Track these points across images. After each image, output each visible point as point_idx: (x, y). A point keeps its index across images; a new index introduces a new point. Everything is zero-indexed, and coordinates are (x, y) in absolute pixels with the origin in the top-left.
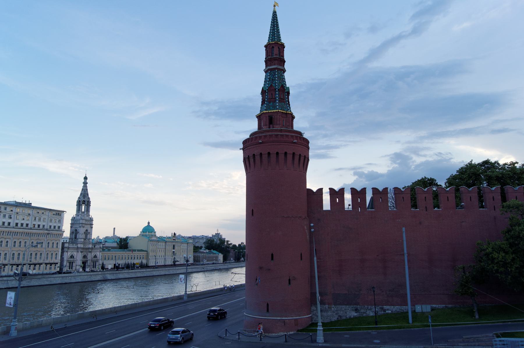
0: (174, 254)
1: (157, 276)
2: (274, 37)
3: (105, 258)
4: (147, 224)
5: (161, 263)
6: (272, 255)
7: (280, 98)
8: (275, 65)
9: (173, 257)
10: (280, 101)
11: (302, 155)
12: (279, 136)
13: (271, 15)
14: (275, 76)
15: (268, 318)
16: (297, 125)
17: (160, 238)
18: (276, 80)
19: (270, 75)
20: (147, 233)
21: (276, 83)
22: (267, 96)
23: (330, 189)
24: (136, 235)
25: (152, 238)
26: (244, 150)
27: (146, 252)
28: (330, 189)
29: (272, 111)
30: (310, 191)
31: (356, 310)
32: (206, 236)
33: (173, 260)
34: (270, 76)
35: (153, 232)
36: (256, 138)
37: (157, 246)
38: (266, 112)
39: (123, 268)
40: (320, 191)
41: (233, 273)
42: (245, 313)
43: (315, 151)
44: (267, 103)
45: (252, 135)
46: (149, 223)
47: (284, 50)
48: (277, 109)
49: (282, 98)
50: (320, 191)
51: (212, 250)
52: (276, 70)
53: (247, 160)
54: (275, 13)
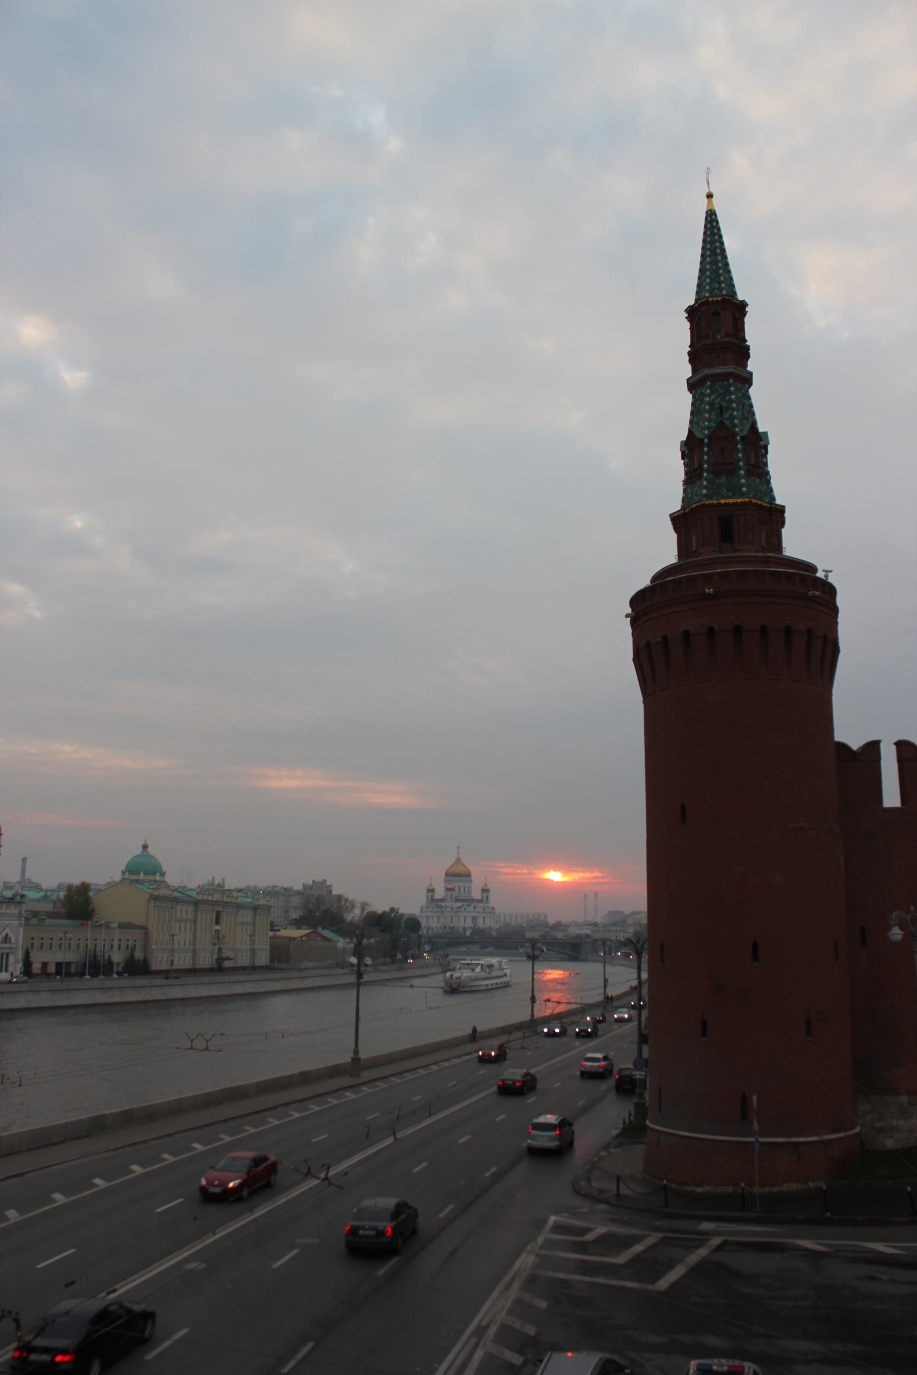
0: (218, 938)
1: (182, 999)
2: (716, 285)
3: (42, 943)
4: (139, 850)
5: (183, 961)
6: (755, 946)
7: (748, 464)
8: (725, 363)
9: (217, 947)
10: (749, 474)
14: (727, 398)
17: (180, 890)
18: (733, 409)
19: (712, 393)
20: (142, 876)
21: (732, 418)
22: (707, 454)
25: (159, 889)
27: (143, 931)
29: (731, 501)
30: (843, 748)
32: (285, 889)
33: (215, 956)
34: (713, 397)
35: (158, 874)
37: (174, 914)
38: (743, 500)
39: (81, 974)
40: (873, 748)
41: (549, 1000)
42: (651, 1122)
44: (711, 476)
45: (659, 577)
46: (145, 847)
48: (742, 495)
50: (873, 748)
52: (731, 380)
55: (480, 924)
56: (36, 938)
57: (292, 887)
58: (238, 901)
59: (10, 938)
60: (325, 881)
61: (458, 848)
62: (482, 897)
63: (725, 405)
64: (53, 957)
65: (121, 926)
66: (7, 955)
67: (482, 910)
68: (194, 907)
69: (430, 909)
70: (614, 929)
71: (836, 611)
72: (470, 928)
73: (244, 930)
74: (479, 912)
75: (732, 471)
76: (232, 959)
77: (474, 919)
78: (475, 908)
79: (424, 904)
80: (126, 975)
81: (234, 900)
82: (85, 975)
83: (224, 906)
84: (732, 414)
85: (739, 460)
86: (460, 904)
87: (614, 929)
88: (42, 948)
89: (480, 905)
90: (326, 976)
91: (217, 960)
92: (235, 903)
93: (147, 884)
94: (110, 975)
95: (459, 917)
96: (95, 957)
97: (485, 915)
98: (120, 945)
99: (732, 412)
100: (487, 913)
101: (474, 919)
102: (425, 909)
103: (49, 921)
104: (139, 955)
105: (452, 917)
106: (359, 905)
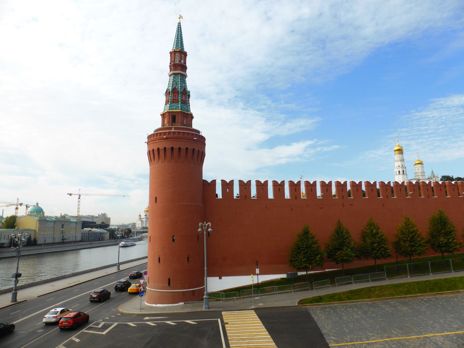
0: (63, 232)
8: (178, 70)
9: (62, 235)
10: (182, 103)
11: (200, 151)
12: (177, 133)
13: (176, 27)
16: (195, 125)
23: (222, 180)
24: (159, 126)
26: (149, 144)
28: (222, 180)
30: (205, 182)
32: (92, 216)
33: (61, 238)
36: (161, 134)
39: (10, 247)
40: (214, 182)
42: (149, 288)
43: (391, 136)
46: (37, 204)
47: (186, 58)
49: (184, 100)
50: (214, 182)
53: (151, 153)
54: (180, 24)
60: (105, 213)
68: (54, 223)
71: (205, 144)
83: (69, 222)
90: (99, 243)
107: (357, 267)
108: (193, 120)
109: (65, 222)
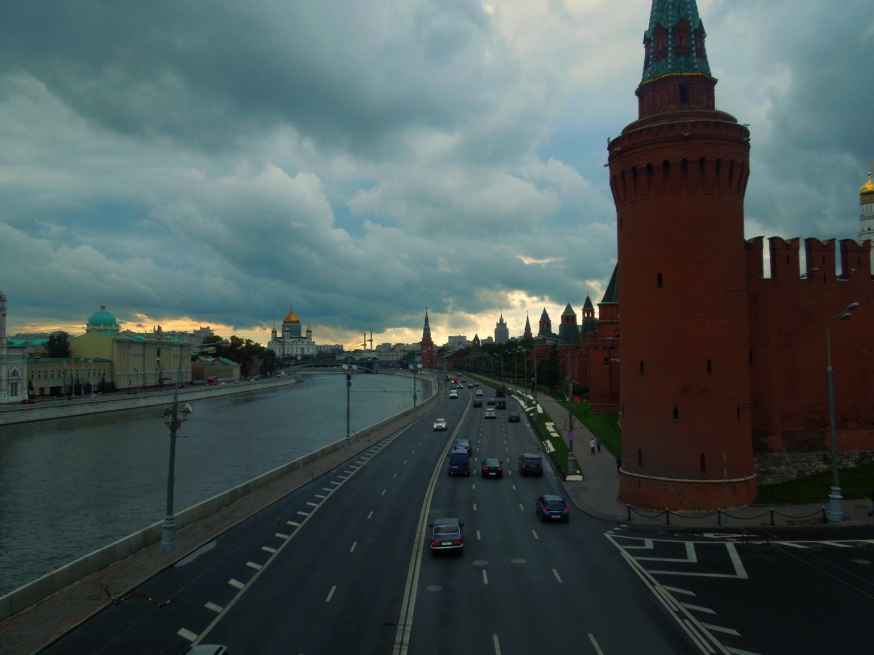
0: (159, 366)
3: (33, 375)
5: (137, 382)
9: (159, 371)
15: (706, 481)
27: (110, 363)
31: (826, 460)
33: (158, 378)
35: (114, 325)
42: (623, 469)
48: (695, 71)
50: (759, 240)
51: (221, 357)
55: (306, 352)
56: (35, 372)
57: (186, 331)
58: (171, 342)
59: (17, 373)
61: (528, 312)
62: (307, 335)
63: (683, 6)
64: (48, 384)
65: (95, 361)
66: (16, 383)
67: (307, 344)
69: (274, 344)
70: (391, 354)
71: (748, 147)
72: (300, 355)
73: (869, 208)
74: (305, 345)
75: (688, 54)
76: (169, 379)
77: (303, 349)
78: (302, 342)
79: (270, 341)
80: (100, 393)
81: (168, 341)
82: (72, 395)
84: (687, 13)
85: (692, 46)
86: (293, 340)
87: (391, 354)
88: (39, 378)
89: (307, 340)
91: (159, 380)
92: (169, 343)
93: (109, 332)
94: (89, 394)
95: (293, 348)
96: (78, 382)
97: (309, 346)
98: (94, 373)
99: (687, 12)
100: (310, 345)
101: (303, 349)
102: (271, 344)
103: (42, 360)
104: (108, 380)
105: (308, 348)
106: (245, 342)
107: (397, 415)
108: (717, 88)
109: (163, 344)
